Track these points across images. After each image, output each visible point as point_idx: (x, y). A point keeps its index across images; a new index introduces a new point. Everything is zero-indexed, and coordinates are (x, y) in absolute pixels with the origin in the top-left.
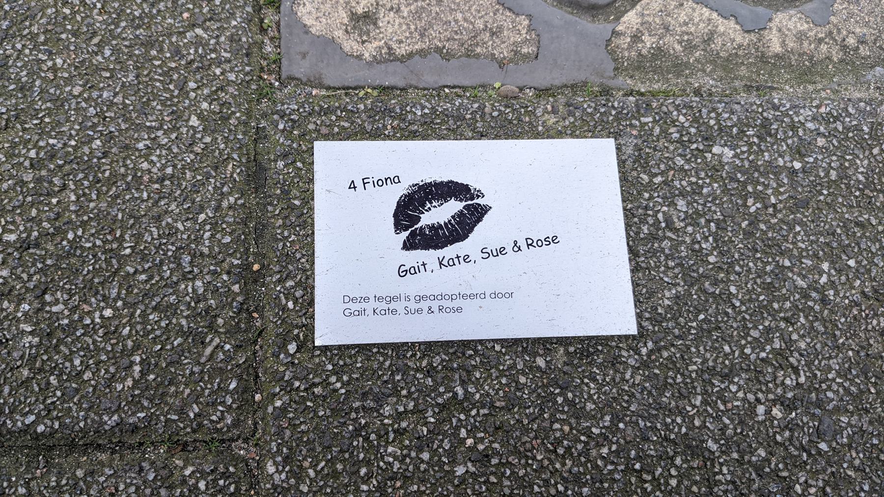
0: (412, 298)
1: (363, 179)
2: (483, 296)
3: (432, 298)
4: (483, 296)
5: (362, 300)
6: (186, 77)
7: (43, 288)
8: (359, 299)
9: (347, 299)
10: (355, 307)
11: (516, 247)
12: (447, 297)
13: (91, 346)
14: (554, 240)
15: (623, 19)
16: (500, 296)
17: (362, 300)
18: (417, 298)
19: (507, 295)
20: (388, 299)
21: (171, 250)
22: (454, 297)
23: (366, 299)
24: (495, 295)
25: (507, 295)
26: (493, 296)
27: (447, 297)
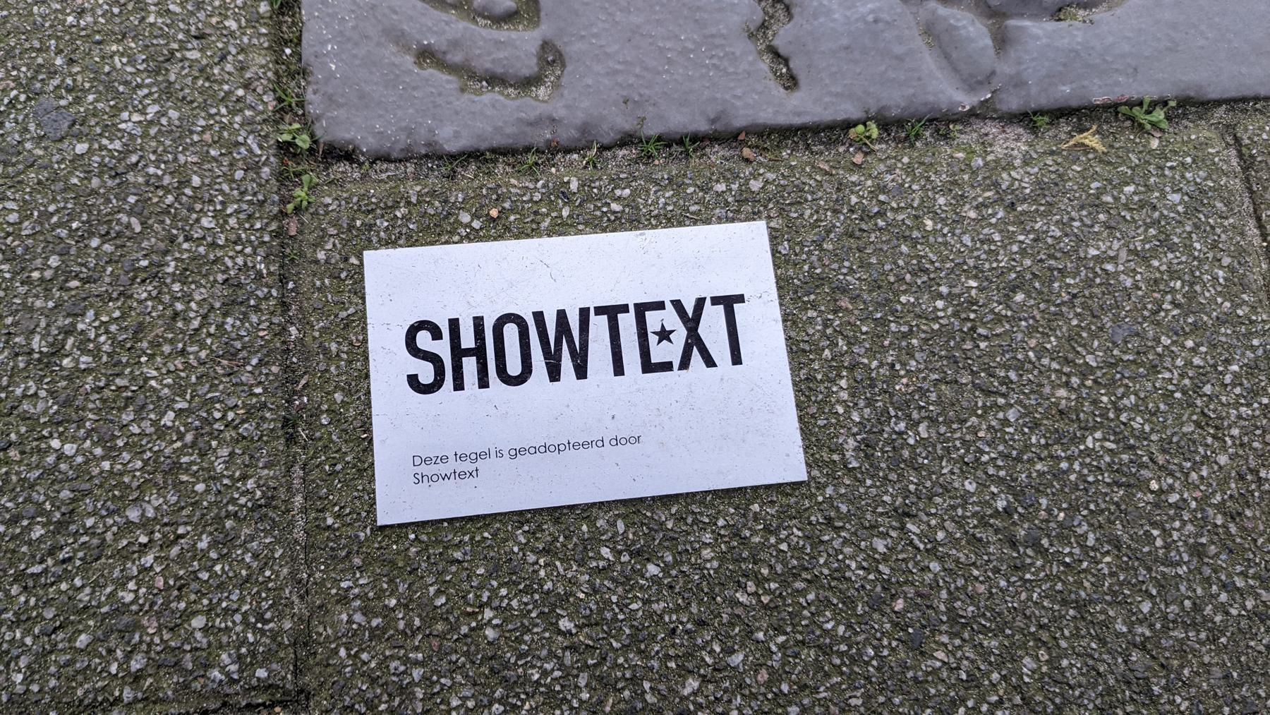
0: (505, 453)
1: (729, 303)
2: (600, 444)
3: (532, 450)
4: (600, 444)
5: (439, 461)
6: (1207, 406)
7: (256, 515)
8: (434, 460)
9: (418, 461)
10: (424, 469)
11: (499, 454)
12: (552, 448)
13: (902, 329)
14: (638, 439)
15: (748, 604)
16: (623, 441)
17: (439, 461)
18: (513, 452)
19: (632, 440)
20: (473, 456)
21: (776, 644)
22: (562, 447)
23: (444, 459)
24: (617, 441)
25: (632, 440)
26: (614, 442)
27: (552, 448)
